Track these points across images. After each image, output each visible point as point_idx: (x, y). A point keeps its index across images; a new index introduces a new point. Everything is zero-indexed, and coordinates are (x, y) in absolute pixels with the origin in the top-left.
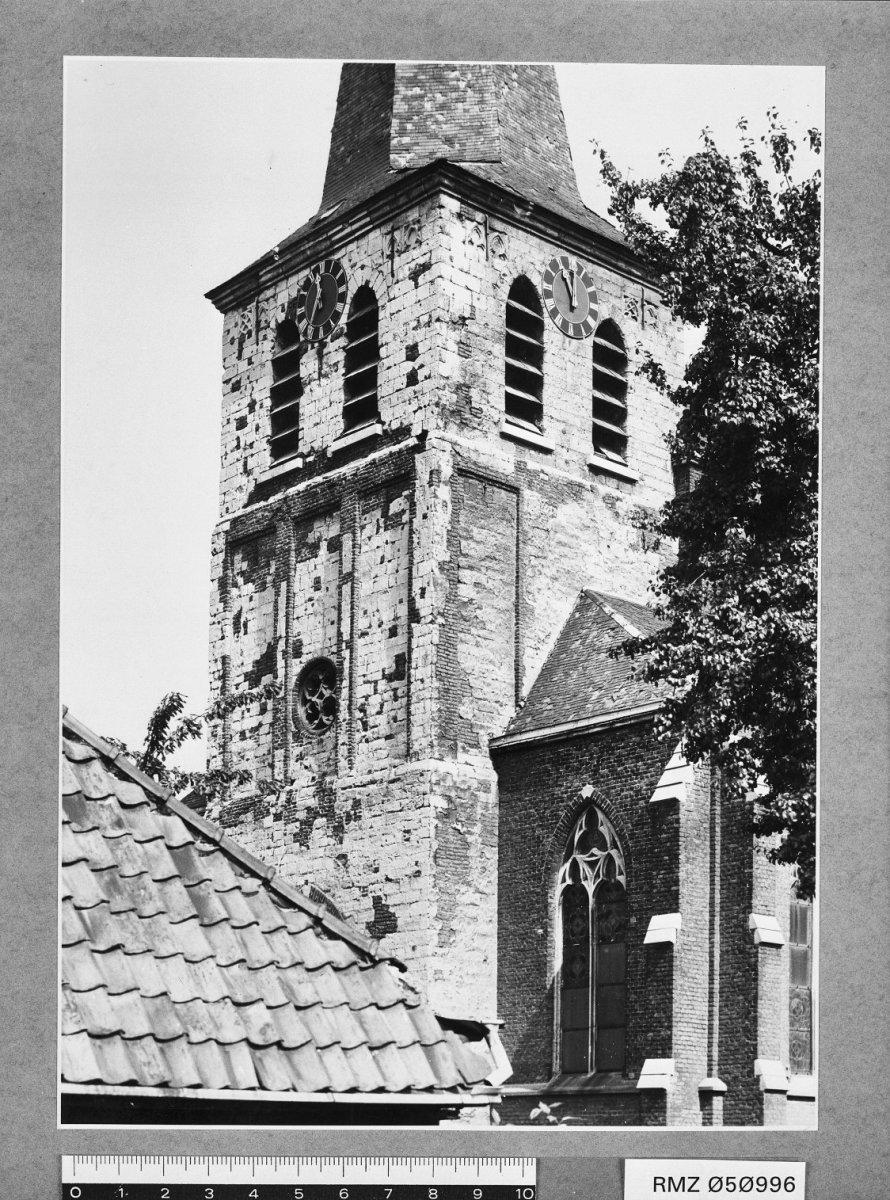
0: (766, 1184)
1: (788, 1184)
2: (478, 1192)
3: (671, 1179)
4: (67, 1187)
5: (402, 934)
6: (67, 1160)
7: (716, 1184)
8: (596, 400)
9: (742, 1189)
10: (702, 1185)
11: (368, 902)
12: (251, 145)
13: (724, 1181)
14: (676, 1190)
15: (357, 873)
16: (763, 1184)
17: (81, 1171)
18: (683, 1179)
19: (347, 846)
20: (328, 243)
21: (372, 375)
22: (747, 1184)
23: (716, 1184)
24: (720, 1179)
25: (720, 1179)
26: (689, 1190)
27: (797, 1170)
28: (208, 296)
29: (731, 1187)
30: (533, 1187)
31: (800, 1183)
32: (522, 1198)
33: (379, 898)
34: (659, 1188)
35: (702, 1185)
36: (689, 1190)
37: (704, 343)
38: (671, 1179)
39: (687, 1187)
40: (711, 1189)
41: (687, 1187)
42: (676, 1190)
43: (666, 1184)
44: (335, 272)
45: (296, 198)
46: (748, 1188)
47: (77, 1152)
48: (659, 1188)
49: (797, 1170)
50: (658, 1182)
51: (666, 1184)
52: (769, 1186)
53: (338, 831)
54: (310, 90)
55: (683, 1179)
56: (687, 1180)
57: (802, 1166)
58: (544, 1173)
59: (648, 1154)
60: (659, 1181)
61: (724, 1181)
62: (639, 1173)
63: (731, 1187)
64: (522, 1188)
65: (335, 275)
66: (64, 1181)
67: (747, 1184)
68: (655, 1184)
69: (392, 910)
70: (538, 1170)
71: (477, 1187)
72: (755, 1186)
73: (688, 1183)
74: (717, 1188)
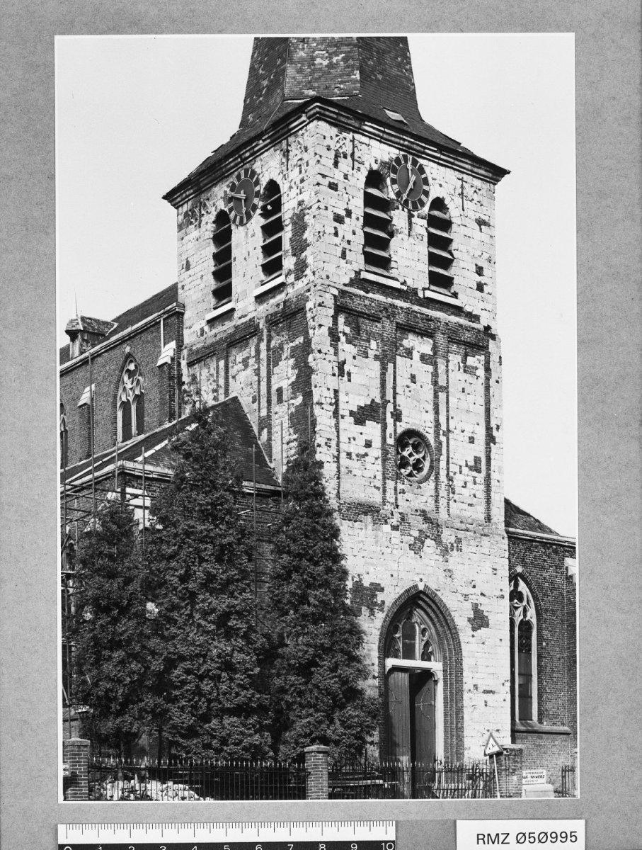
0: (557, 836)
1: (573, 836)
2: (354, 846)
3: (489, 835)
4: (61, 847)
5: (492, 630)
6: (61, 828)
7: (522, 838)
8: (431, 273)
9: (540, 841)
10: (512, 839)
11: (468, 605)
12: (195, 89)
13: (527, 835)
14: (493, 843)
15: (458, 582)
16: (554, 837)
17: (70, 835)
18: (498, 835)
19: (450, 566)
20: (422, 150)
21: (229, 249)
22: (543, 838)
23: (522, 838)
24: (524, 834)
25: (524, 834)
26: (502, 843)
27: (578, 826)
28: (169, 197)
29: (532, 840)
30: (393, 842)
31: (581, 835)
32: (386, 849)
33: (477, 604)
34: (481, 842)
35: (512, 839)
36: (502, 843)
37: (214, 266)
38: (489, 835)
39: (501, 840)
40: (518, 842)
41: (501, 840)
42: (493, 843)
43: (486, 839)
44: (252, 177)
45: (225, 124)
46: (544, 840)
47: (72, 822)
48: (481, 842)
49: (578, 826)
50: (480, 838)
51: (486, 839)
52: (559, 838)
53: (445, 551)
54: (231, 58)
55: (498, 835)
56: (500, 835)
57: (583, 822)
58: (537, 815)
59: (482, 817)
60: (481, 837)
61: (527, 835)
62: (467, 831)
63: (532, 840)
64: (386, 842)
65: (252, 179)
66: (59, 843)
67: (543, 838)
68: (478, 839)
69: (485, 614)
70: (397, 831)
71: (354, 842)
72: (549, 838)
73: (502, 838)
74: (522, 840)
